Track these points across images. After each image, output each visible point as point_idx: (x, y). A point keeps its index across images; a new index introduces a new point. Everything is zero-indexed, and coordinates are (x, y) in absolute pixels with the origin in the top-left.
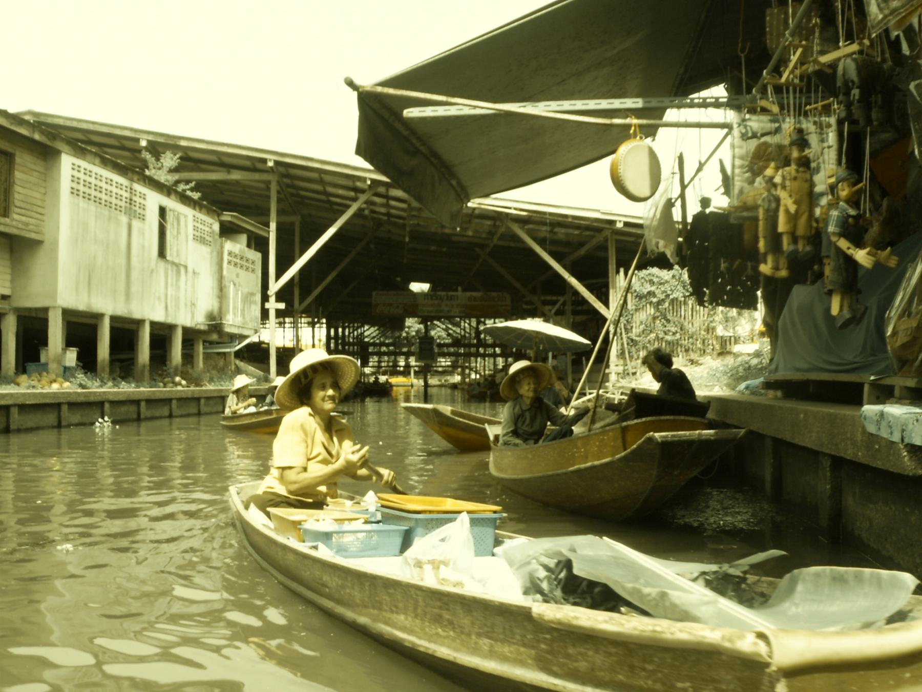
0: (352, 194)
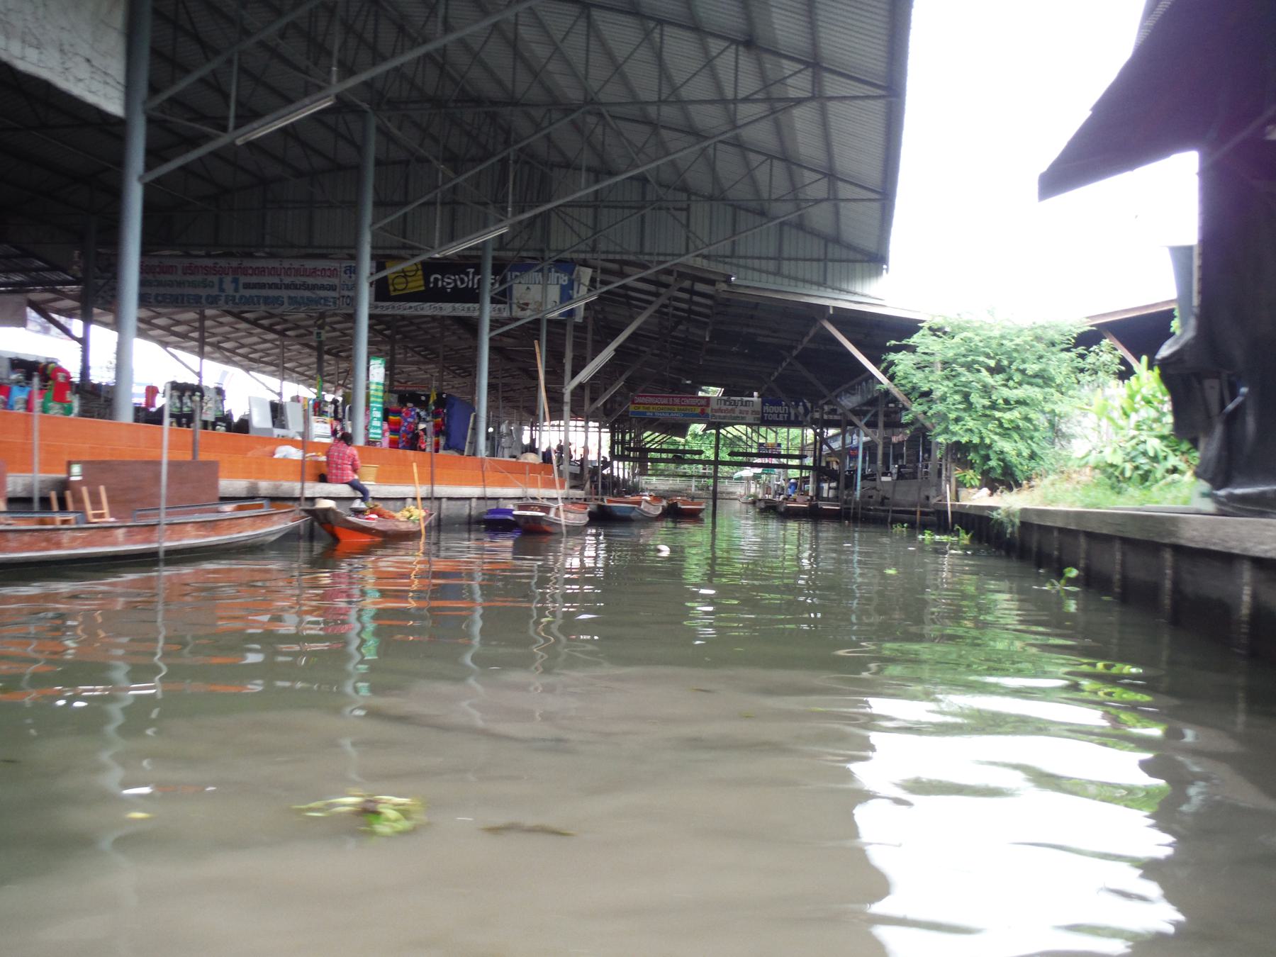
0: (652, 288)
